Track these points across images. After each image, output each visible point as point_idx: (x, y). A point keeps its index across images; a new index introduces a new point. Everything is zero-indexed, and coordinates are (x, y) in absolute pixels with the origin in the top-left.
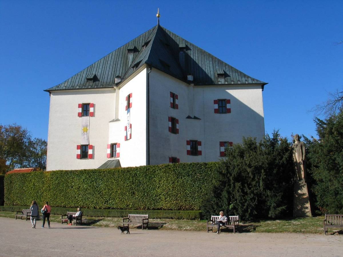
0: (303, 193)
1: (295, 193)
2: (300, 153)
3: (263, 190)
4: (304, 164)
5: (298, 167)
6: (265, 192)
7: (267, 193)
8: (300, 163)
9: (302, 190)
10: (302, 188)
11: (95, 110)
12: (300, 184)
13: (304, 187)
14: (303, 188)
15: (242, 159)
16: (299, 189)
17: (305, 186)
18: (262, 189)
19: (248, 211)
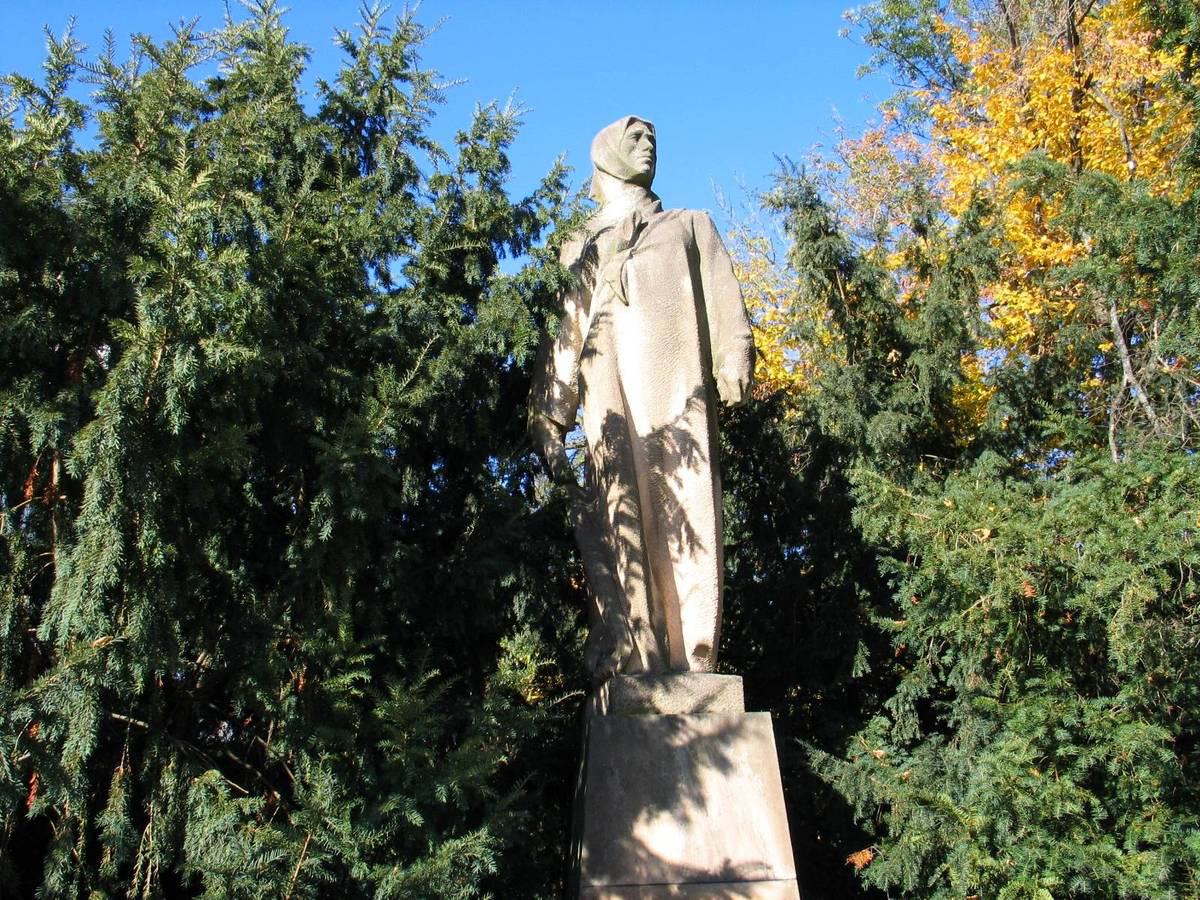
0: (711, 864)
1: (597, 867)
2: (673, 319)
3: (98, 769)
4: (721, 466)
5: (643, 482)
6: (138, 816)
7: (176, 836)
8: (671, 446)
9: (700, 801)
10: (695, 781)
11: (698, 322)
12: (673, 723)
13: (724, 765)
14: (710, 776)
15: (996, 472)
16: (664, 799)
17: (737, 752)
18: (79, 744)
19: (561, 720)
